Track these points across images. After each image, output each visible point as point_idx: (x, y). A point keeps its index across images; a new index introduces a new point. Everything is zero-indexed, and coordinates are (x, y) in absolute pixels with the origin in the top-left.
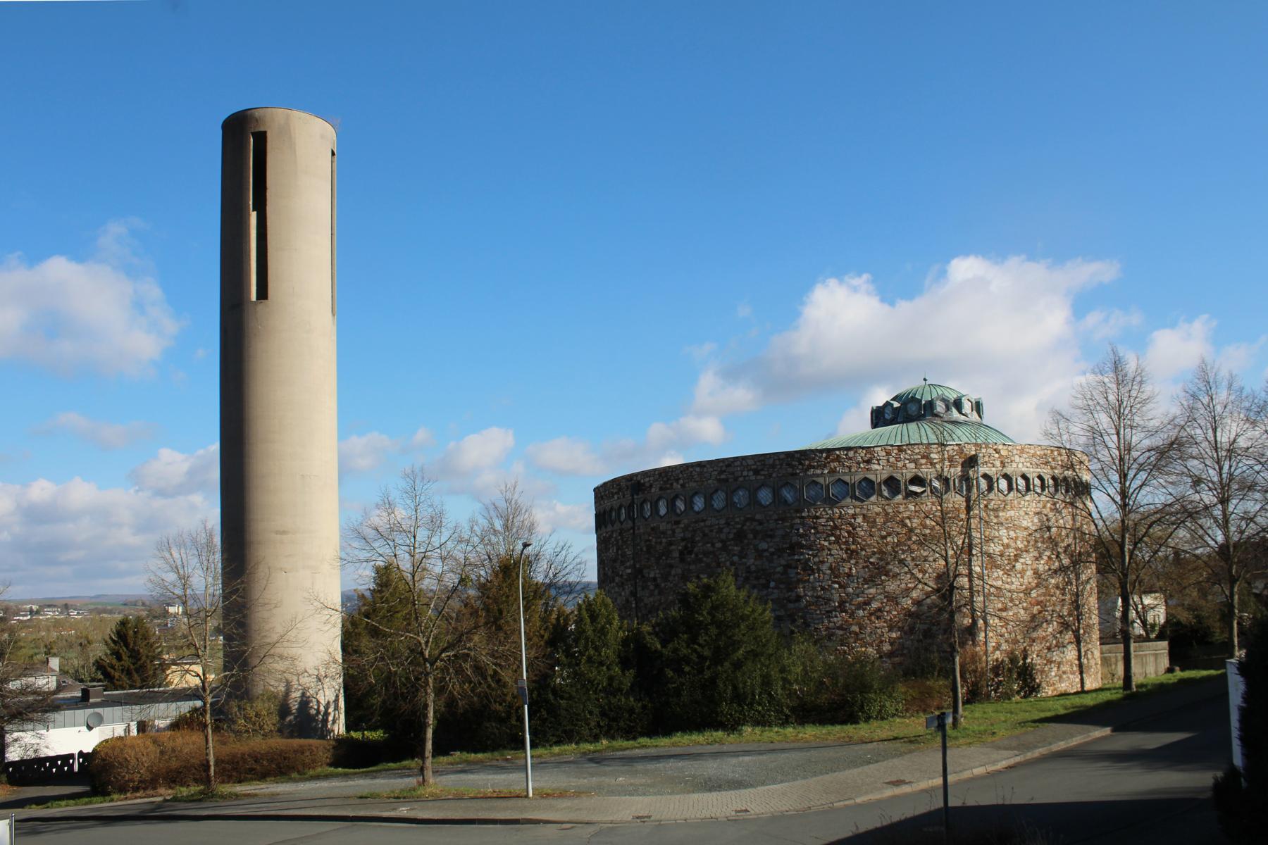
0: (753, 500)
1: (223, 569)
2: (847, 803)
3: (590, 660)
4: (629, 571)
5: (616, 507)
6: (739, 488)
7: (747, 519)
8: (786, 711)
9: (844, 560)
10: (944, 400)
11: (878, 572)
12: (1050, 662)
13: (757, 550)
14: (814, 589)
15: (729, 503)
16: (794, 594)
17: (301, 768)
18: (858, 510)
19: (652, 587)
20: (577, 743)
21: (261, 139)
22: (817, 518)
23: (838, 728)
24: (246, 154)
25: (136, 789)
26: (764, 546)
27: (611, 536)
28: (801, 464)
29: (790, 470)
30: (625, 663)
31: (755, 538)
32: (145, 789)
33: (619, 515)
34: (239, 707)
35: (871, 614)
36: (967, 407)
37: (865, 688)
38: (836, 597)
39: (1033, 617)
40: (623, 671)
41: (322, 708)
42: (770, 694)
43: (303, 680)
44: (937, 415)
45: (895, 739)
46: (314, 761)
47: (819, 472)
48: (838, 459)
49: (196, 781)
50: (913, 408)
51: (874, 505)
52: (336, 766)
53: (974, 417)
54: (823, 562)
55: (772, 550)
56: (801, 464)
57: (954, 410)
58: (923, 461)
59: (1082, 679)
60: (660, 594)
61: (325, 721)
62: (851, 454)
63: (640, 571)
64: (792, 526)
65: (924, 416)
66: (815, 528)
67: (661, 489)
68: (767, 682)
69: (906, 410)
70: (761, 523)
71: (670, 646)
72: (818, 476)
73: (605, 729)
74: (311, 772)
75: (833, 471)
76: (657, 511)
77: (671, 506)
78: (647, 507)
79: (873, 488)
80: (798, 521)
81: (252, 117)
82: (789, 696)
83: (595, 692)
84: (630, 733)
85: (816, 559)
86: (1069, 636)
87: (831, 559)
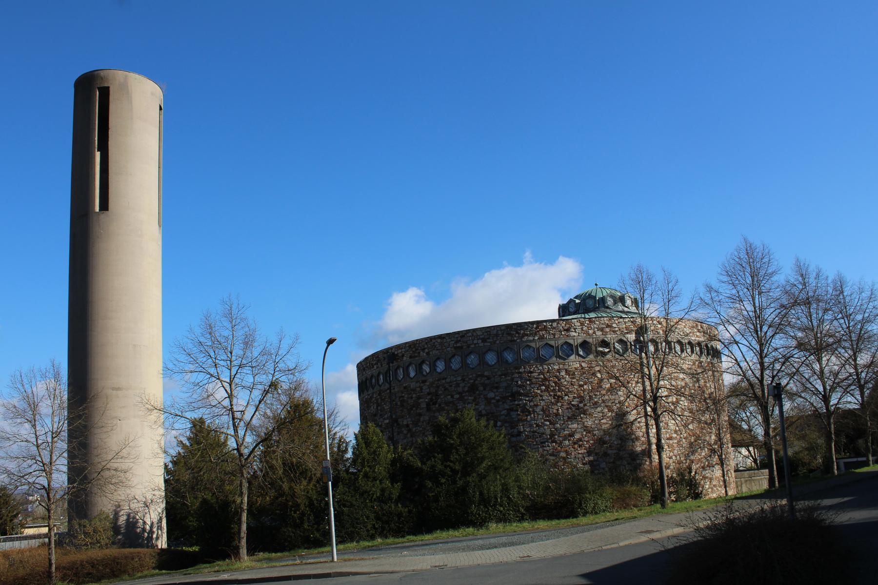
0: (482, 362)
1: (69, 400)
2: (613, 546)
3: (366, 476)
4: (387, 421)
5: (375, 374)
6: (471, 353)
7: (478, 376)
8: (522, 510)
9: (553, 404)
10: (612, 296)
11: (577, 412)
12: (705, 478)
13: (486, 398)
14: (531, 426)
15: (464, 364)
16: (516, 431)
17: (130, 571)
18: (561, 366)
19: (405, 432)
20: (358, 542)
21: (105, 93)
22: (531, 372)
23: (563, 521)
24: (92, 109)
26: (491, 395)
27: (371, 398)
28: (517, 333)
29: (509, 338)
30: (393, 478)
31: (485, 389)
33: (378, 380)
34: (80, 525)
35: (575, 443)
36: (628, 302)
37: (581, 490)
38: (548, 432)
39: (691, 444)
40: (392, 484)
41: (148, 527)
42: (509, 498)
43: (133, 506)
44: (608, 308)
45: (617, 519)
46: (142, 566)
47: (531, 338)
48: (545, 328)
50: (590, 303)
51: (574, 363)
52: (160, 569)
53: (633, 309)
54: (536, 405)
55: (497, 398)
56: (517, 333)
57: (620, 304)
58: (608, 330)
59: (726, 491)
60: (411, 436)
61: (150, 538)
62: (555, 325)
63: (396, 421)
64: (512, 380)
65: (598, 308)
66: (530, 380)
67: (411, 357)
68: (506, 489)
69: (585, 304)
70: (489, 378)
71: (429, 463)
72: (531, 341)
73: (379, 530)
74: (139, 574)
75: (542, 338)
76: (408, 374)
77: (419, 369)
78: (401, 372)
79: (572, 350)
80: (517, 375)
82: (523, 499)
83: (371, 501)
84: (399, 532)
85: (532, 404)
86: (716, 459)
87: (543, 403)
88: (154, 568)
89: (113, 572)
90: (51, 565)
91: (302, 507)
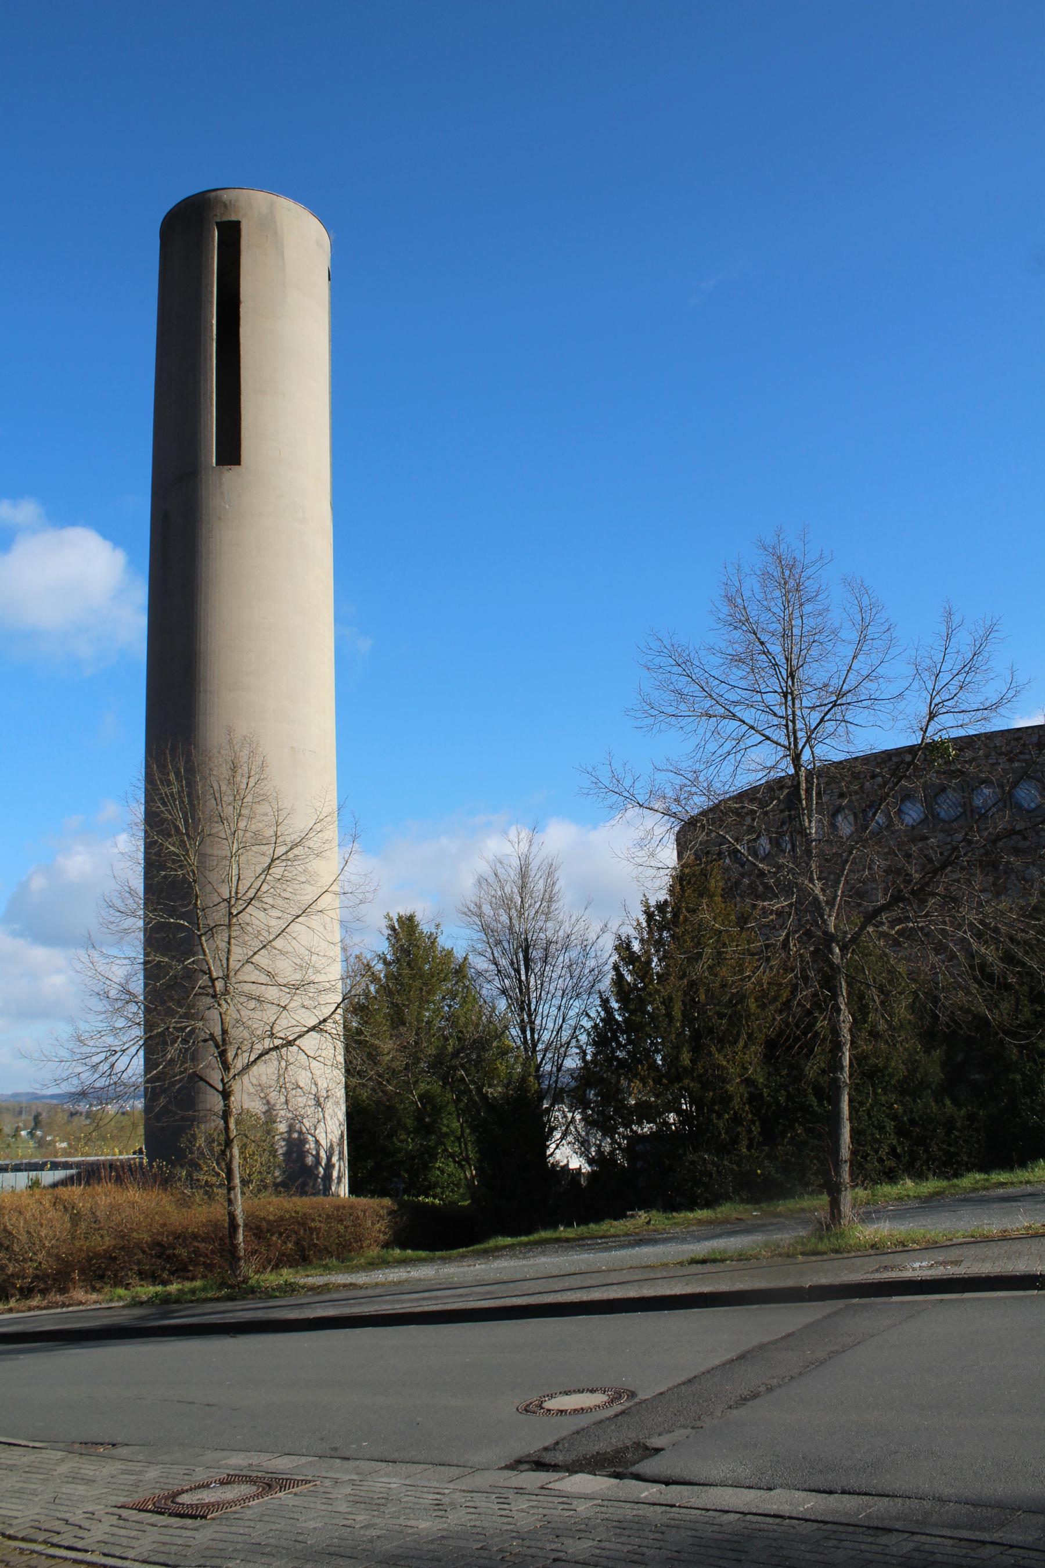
21: (231, 234)
24: (200, 266)
25: (27, 1293)
32: (44, 1292)
41: (323, 1154)
49: (143, 1275)
52: (403, 1247)
73: (905, 1159)
81: (218, 201)
84: (950, 1166)
88: (386, 1245)
89: (302, 1249)
90: (233, 1226)
91: (736, 1103)
